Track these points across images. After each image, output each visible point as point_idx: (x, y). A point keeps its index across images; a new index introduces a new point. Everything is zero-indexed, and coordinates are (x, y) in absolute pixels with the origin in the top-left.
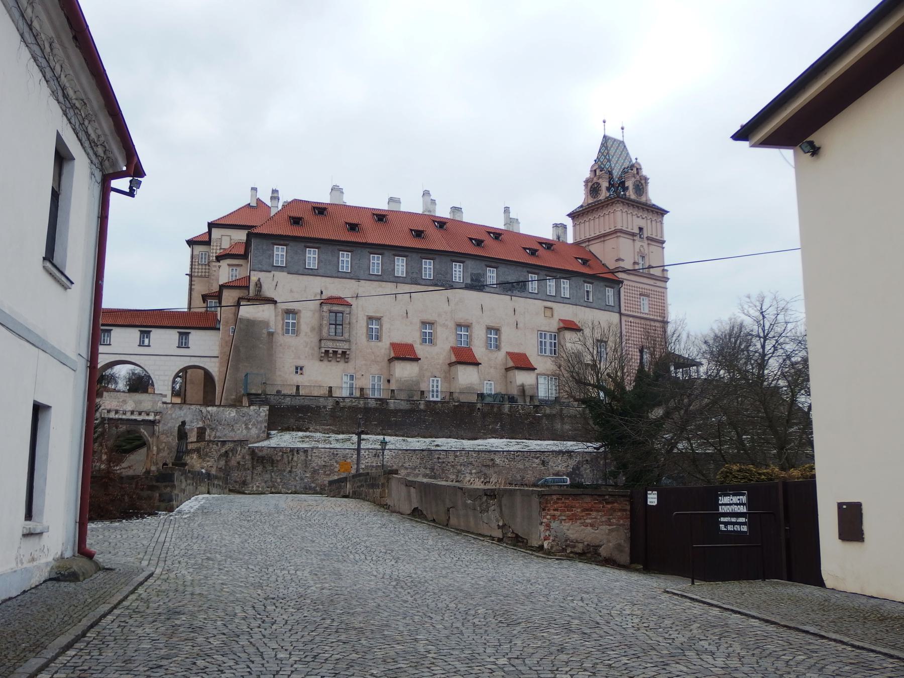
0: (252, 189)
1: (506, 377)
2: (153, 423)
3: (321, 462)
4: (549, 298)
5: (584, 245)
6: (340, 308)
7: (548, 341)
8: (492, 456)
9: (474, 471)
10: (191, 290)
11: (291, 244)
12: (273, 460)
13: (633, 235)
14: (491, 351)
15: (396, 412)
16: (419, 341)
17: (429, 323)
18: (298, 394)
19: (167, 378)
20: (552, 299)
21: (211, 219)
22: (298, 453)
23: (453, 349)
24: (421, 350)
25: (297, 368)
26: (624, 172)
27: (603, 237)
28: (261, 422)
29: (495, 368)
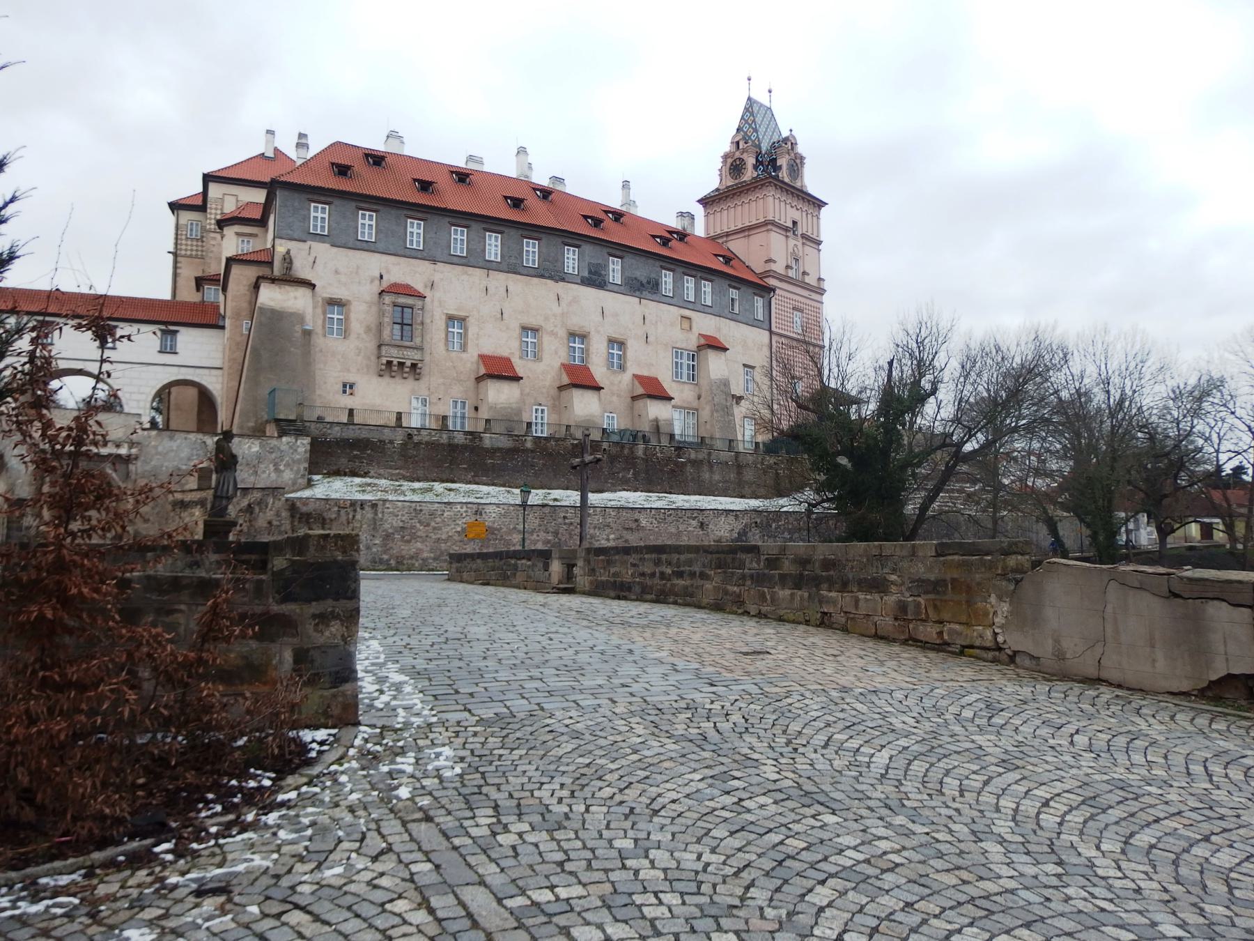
0: (268, 132)
1: (632, 408)
2: (128, 460)
3: (397, 523)
4: (685, 305)
5: (720, 241)
6: (410, 301)
7: (685, 361)
8: (637, 515)
9: (612, 536)
10: (175, 275)
11: (337, 202)
12: (324, 519)
13: (786, 229)
14: (614, 372)
15: (494, 451)
16: (517, 354)
17: (532, 329)
18: (351, 422)
19: (144, 397)
20: (691, 306)
21: (211, 168)
22: (362, 508)
23: (563, 365)
24: (520, 367)
25: (345, 386)
26: (773, 146)
27: (747, 231)
28: (299, 462)
29: (619, 396)
